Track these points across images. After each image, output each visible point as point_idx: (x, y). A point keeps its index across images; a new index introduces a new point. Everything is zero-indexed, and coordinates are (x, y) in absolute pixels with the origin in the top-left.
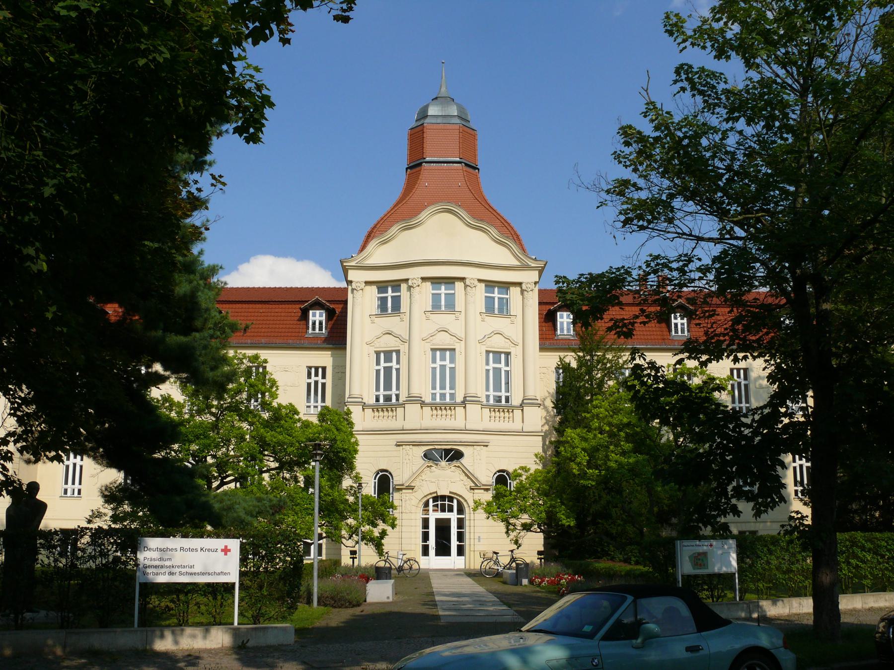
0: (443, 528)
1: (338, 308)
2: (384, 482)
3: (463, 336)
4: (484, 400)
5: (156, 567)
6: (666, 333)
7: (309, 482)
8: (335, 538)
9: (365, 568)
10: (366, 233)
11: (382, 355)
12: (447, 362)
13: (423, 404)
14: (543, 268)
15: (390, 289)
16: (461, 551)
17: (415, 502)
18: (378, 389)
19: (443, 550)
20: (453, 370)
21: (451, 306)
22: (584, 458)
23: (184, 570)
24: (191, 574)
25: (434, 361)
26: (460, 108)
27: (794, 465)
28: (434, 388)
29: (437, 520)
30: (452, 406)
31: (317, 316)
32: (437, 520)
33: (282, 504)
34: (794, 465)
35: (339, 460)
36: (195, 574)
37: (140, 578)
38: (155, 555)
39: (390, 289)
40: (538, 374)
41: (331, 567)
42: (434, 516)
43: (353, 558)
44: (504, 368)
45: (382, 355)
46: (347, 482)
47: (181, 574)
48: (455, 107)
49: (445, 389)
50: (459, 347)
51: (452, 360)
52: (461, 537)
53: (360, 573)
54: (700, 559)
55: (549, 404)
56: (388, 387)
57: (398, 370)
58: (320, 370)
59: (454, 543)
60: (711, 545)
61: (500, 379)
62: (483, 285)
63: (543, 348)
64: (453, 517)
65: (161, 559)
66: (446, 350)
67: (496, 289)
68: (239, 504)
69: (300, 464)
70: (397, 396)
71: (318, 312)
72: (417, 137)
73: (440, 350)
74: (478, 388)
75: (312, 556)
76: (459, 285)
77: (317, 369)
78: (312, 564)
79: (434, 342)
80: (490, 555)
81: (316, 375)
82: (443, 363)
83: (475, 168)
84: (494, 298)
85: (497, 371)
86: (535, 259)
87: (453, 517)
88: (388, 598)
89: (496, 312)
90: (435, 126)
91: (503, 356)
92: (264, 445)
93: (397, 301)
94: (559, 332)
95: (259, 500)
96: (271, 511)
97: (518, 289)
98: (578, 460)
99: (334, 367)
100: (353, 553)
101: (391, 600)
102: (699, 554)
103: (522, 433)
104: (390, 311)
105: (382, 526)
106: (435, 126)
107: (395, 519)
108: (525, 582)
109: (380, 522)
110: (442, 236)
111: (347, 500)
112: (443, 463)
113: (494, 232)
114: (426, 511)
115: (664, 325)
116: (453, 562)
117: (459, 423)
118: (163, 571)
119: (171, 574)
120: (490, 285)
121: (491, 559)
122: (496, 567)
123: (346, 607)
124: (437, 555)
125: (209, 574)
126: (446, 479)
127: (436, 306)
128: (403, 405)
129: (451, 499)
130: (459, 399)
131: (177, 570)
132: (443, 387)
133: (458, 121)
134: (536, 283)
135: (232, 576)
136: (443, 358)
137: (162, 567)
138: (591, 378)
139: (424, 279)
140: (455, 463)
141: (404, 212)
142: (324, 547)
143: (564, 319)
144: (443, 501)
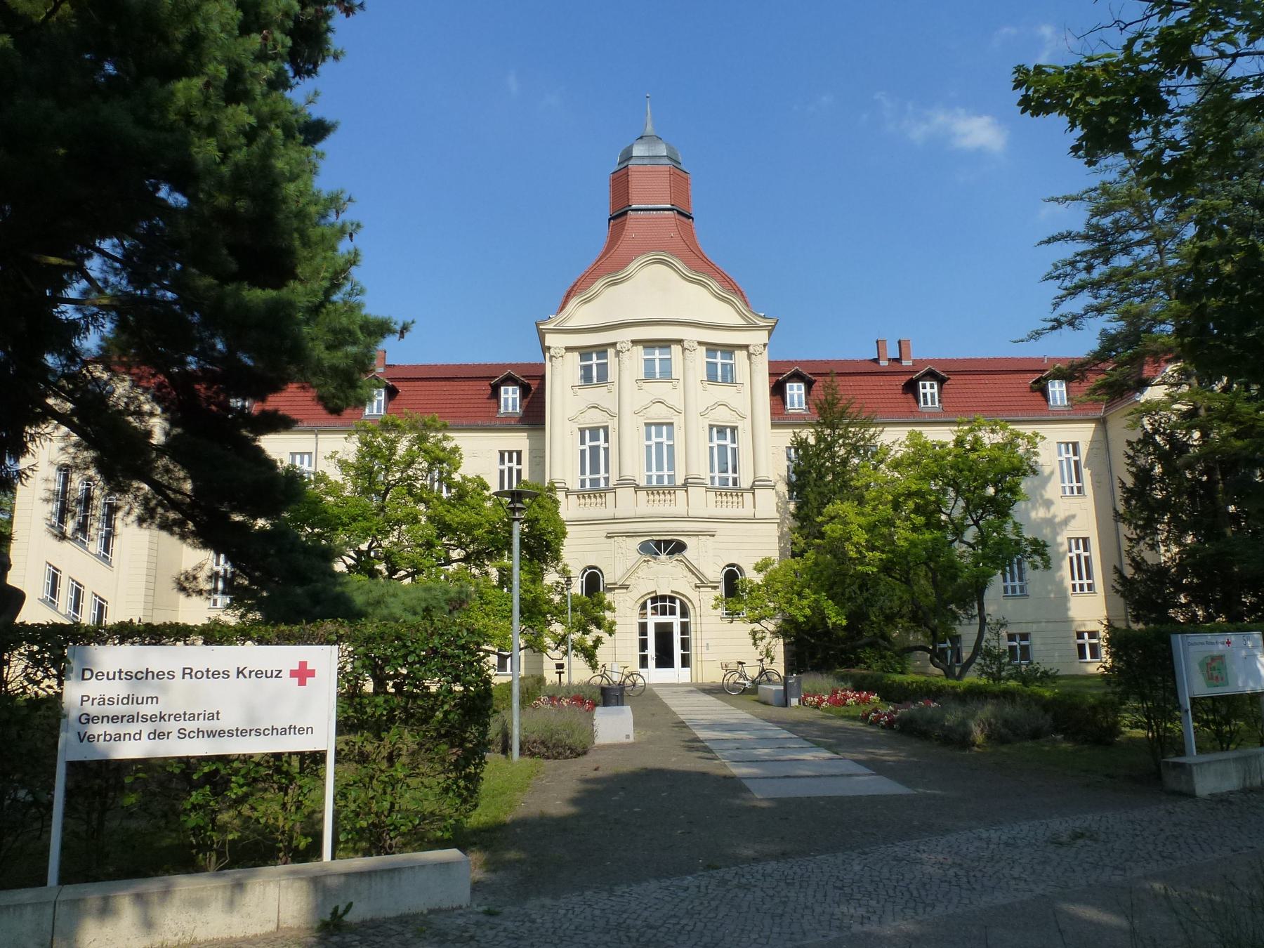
0: (664, 634)
1: (534, 385)
2: (593, 580)
3: (682, 408)
4: (708, 481)
5: (114, 719)
6: (913, 404)
7: (505, 580)
8: (536, 647)
9: (579, 686)
10: (565, 293)
11: (587, 432)
12: (664, 439)
13: (637, 488)
14: (773, 327)
15: (594, 356)
16: (686, 662)
17: (630, 603)
18: (583, 472)
19: (665, 659)
20: (671, 447)
21: (667, 374)
22: (861, 537)
23: (191, 726)
24: (211, 734)
25: (649, 437)
26: (669, 148)
27: (1070, 554)
28: (649, 469)
29: (658, 625)
30: (672, 489)
31: (510, 396)
32: (658, 625)
33: (463, 596)
34: (1070, 554)
35: (542, 548)
36: (221, 733)
37: (68, 749)
38: (118, 689)
39: (594, 356)
40: (770, 453)
41: (533, 688)
42: (652, 620)
43: (560, 673)
44: (730, 446)
45: (587, 432)
46: (551, 578)
47: (182, 734)
48: (664, 146)
50: (678, 421)
51: (670, 436)
52: (685, 644)
53: (573, 694)
54: (1215, 668)
55: (783, 488)
56: (595, 469)
57: (606, 449)
58: (515, 455)
60: (1228, 643)
61: (726, 461)
62: (704, 348)
63: (774, 426)
64: (676, 620)
65: (130, 699)
66: (662, 424)
67: (719, 354)
68: (395, 596)
69: (490, 556)
70: (607, 479)
71: (510, 388)
72: (621, 181)
73: (656, 424)
74: (701, 468)
75: (509, 671)
76: (676, 349)
77: (511, 453)
78: (509, 686)
79: (712, 417)
80: (734, 666)
81: (510, 460)
82: (659, 440)
83: (689, 217)
84: (716, 364)
85: (723, 449)
86: (764, 317)
87: (676, 620)
88: (628, 737)
89: (720, 379)
90: (641, 168)
91: (728, 431)
92: (444, 528)
93: (603, 368)
94: (788, 406)
95: (428, 590)
96: (447, 608)
97: (745, 353)
98: (855, 539)
99: (531, 451)
100: (560, 666)
101: (632, 740)
102: (1213, 659)
103: (753, 520)
104: (595, 381)
105: (595, 632)
106: (641, 168)
107: (613, 623)
108: (794, 701)
109: (593, 628)
110: (656, 291)
111: (552, 600)
112: (663, 557)
113: (715, 285)
114: (644, 615)
115: (910, 396)
116: (676, 674)
117: (680, 509)
118: (133, 728)
119: (158, 735)
120: (712, 348)
121: (736, 671)
122: (742, 681)
123: (567, 758)
125: (258, 733)
126: (666, 576)
127: (649, 375)
128: (613, 490)
129: (672, 599)
130: (679, 482)
131: (173, 726)
132: (660, 468)
133: (667, 161)
134: (765, 345)
135: (321, 735)
136: (659, 435)
137: (131, 719)
138: (833, 456)
139: (635, 342)
140: (677, 556)
141: (610, 264)
142: (522, 659)
143: (795, 391)
144: (663, 603)
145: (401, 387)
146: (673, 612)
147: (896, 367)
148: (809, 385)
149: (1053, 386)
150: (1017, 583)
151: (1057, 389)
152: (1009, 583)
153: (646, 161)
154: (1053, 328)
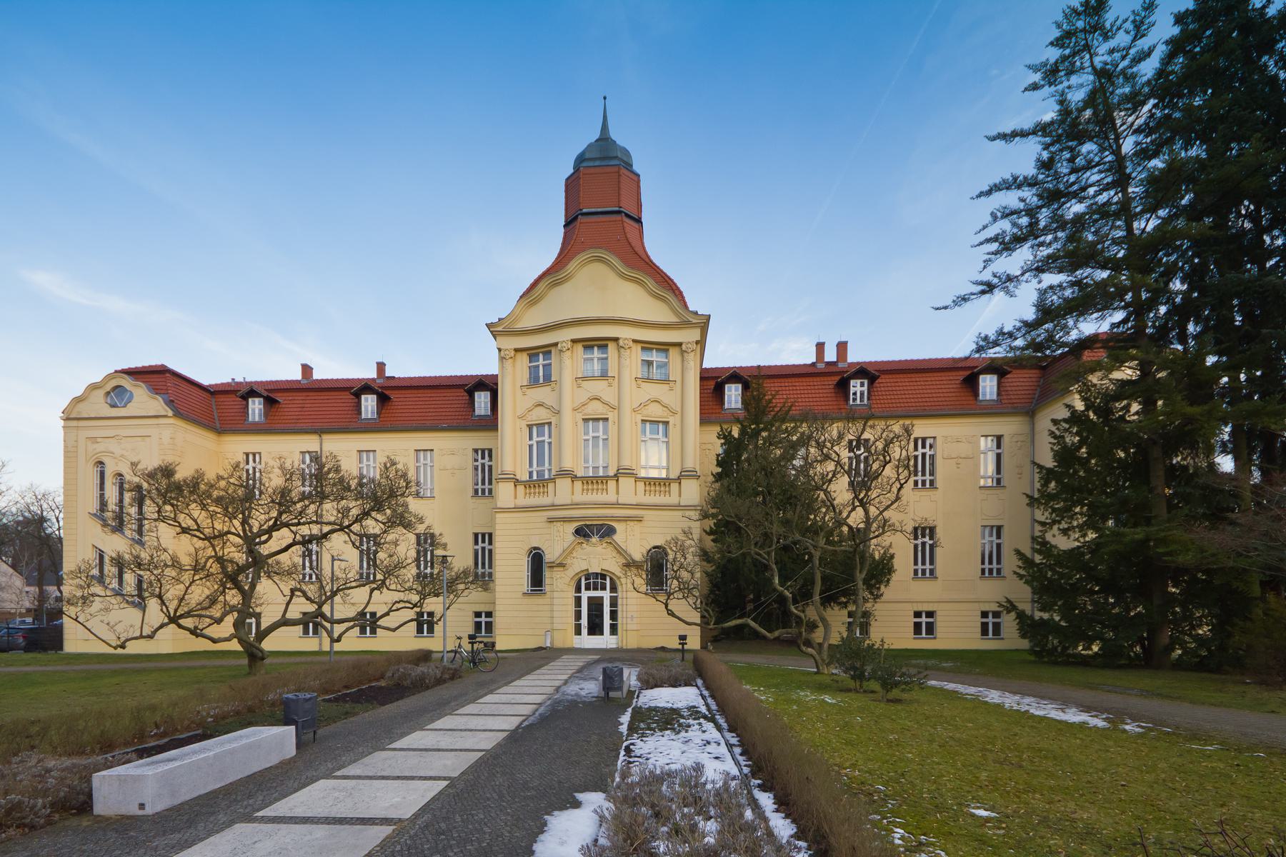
0: (595, 605)
13: (517, 482)
15: (541, 356)
16: (614, 629)
19: (595, 628)
29: (589, 598)
32: (589, 598)
42: (585, 595)
45: (535, 429)
49: (543, 465)
50: (612, 416)
52: (614, 615)
57: (550, 443)
59: (607, 621)
64: (606, 595)
70: (550, 470)
79: (645, 412)
106: (592, 171)
113: (650, 283)
114: (578, 589)
117: (610, 497)
120: (647, 346)
124: (589, 634)
126: (597, 557)
129: (603, 577)
144: (596, 580)
145: (393, 395)
146: (604, 588)
147: (833, 369)
148: (746, 387)
149: (984, 381)
150: (928, 566)
151: (988, 385)
152: (920, 566)
153: (597, 163)
154: (983, 292)
